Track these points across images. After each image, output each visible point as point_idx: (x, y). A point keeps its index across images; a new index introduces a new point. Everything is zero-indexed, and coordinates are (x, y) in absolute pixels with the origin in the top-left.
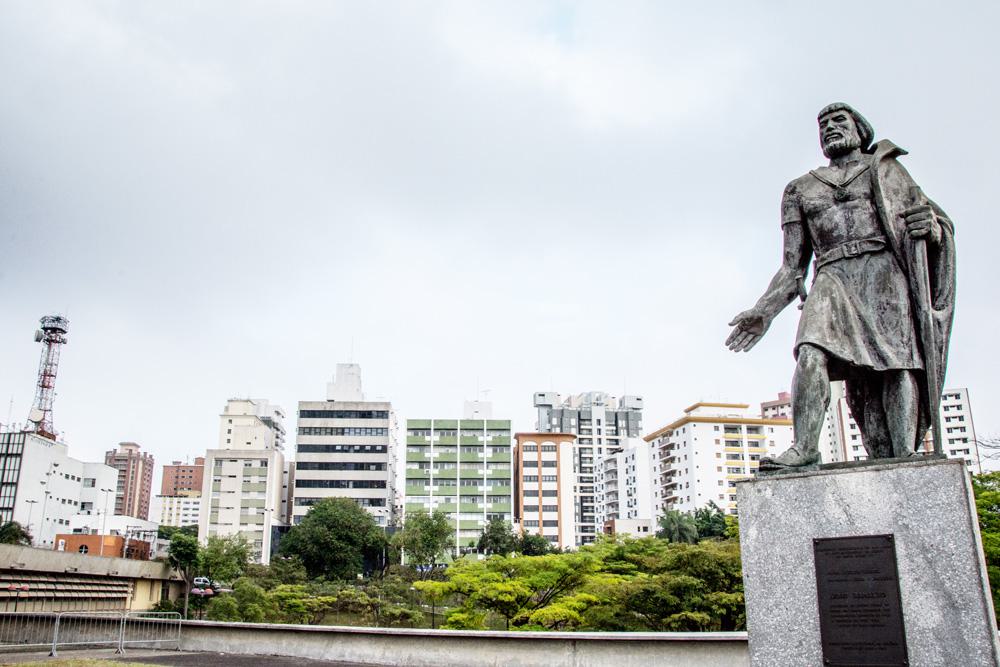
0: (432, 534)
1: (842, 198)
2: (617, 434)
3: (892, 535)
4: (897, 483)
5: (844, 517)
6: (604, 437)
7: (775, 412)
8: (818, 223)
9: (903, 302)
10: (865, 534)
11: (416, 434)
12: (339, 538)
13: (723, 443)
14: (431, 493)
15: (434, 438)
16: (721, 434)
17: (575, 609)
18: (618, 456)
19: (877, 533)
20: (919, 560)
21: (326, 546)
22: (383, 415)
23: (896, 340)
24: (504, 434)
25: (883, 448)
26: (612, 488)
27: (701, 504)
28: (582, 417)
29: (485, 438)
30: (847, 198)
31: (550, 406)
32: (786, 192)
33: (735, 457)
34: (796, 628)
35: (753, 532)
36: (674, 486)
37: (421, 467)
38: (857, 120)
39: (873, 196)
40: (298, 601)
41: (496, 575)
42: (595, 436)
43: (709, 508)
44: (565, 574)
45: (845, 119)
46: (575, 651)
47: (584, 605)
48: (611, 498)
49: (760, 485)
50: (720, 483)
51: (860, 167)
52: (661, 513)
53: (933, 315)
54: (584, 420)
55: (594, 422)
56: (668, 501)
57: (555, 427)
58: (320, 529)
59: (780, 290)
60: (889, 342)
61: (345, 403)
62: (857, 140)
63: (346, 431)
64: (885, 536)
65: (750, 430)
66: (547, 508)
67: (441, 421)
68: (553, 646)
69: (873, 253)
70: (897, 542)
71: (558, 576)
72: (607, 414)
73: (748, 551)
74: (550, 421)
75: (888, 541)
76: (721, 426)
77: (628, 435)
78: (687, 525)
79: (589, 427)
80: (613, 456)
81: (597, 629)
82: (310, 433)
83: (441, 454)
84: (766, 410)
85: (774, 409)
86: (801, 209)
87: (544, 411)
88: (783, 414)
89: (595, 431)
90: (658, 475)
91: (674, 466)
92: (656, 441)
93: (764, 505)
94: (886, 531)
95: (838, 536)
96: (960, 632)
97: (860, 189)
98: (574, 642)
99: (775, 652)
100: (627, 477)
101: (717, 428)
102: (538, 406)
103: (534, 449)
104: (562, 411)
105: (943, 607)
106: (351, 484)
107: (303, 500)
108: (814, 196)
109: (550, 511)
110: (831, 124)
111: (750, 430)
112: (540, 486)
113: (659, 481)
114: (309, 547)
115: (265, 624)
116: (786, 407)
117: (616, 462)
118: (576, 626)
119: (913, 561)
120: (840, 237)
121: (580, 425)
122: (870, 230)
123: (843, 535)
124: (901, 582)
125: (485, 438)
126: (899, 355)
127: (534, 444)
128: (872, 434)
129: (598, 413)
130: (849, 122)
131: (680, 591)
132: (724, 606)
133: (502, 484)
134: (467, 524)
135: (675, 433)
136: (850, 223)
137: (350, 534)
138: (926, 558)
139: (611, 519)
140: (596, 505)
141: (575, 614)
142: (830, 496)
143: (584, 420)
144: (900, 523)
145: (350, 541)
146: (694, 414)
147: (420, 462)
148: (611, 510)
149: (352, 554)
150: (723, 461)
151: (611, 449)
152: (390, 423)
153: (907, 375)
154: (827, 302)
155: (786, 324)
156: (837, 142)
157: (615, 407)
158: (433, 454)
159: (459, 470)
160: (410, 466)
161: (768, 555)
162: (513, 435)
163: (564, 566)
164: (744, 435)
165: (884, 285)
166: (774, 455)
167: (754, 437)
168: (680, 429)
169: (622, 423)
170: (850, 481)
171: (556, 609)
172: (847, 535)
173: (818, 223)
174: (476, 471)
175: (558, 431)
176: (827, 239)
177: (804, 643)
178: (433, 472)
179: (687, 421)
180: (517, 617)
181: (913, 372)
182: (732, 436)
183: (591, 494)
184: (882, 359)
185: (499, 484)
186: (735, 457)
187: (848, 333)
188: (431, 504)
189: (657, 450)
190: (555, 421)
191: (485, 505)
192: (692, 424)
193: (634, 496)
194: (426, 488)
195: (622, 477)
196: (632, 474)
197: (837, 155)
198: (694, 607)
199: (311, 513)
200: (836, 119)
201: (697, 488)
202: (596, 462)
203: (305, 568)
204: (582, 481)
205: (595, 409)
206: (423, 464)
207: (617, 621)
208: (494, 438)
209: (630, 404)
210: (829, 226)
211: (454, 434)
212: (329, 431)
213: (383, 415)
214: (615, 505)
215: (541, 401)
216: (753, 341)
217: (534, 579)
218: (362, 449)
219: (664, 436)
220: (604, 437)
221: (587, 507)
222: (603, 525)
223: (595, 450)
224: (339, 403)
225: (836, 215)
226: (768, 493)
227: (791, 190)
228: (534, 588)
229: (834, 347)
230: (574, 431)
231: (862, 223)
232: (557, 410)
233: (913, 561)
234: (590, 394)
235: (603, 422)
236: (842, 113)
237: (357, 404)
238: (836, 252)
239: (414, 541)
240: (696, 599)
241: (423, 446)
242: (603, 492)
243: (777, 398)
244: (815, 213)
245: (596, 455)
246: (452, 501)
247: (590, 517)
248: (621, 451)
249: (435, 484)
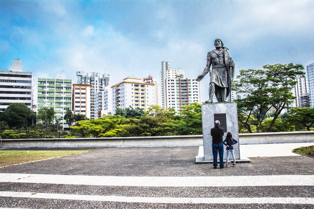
0: (50, 113)
1: (218, 56)
2: (102, 85)
4: (227, 106)
5: (219, 111)
6: (98, 86)
7: (147, 81)
8: (214, 60)
9: (226, 76)
11: (41, 83)
12: (20, 115)
13: (134, 89)
14: (46, 102)
15: (47, 84)
16: (134, 87)
17: (115, 133)
18: (102, 92)
20: (229, 117)
21: (15, 118)
22: (30, 76)
23: (225, 82)
24: (70, 84)
25: (221, 100)
26: (100, 101)
27: (127, 106)
28: (91, 80)
29: (64, 85)
30: (220, 57)
31: (82, 76)
32: (208, 53)
33: (137, 93)
35: (204, 113)
36: (119, 101)
37: (43, 93)
38: (222, 42)
39: (224, 57)
40: (13, 135)
41: (94, 124)
42: (95, 86)
43: (129, 108)
44: (111, 124)
46: (124, 142)
47: (117, 132)
48: (100, 104)
49: (206, 105)
50: (132, 101)
51: (222, 51)
52: (116, 109)
54: (92, 81)
55: (95, 81)
56: (117, 105)
57: (83, 82)
58: (13, 113)
59: (206, 71)
60: (224, 82)
61: (16, 72)
62: (221, 46)
63: (17, 81)
65: (142, 86)
66: (82, 107)
67: (49, 79)
68: (118, 141)
69: (223, 67)
71: (110, 124)
72: (99, 79)
74: (81, 80)
75: (225, 114)
76: (134, 84)
77: (105, 85)
78: (123, 112)
79: (93, 83)
80: (101, 92)
81: (122, 137)
82: (3, 82)
83: (49, 89)
85: (147, 80)
86: (211, 57)
87: (80, 77)
88: (149, 82)
89: (95, 84)
90: (115, 97)
91: (119, 95)
92: (114, 88)
93: (206, 108)
94: (225, 113)
97: (222, 56)
98: (123, 140)
100: (105, 98)
101: (132, 85)
102: (78, 75)
103: (79, 89)
104: (85, 77)
106: (19, 98)
107: (2, 103)
108: (214, 55)
109: (83, 107)
110: (218, 42)
112: (80, 100)
113: (115, 100)
114: (9, 118)
115: (22, 139)
116: (150, 80)
117: (101, 93)
118: (114, 136)
120: (218, 64)
121: (91, 82)
122: (223, 63)
125: (64, 85)
126: (225, 85)
127: (79, 87)
128: (218, 97)
129: (96, 79)
130: (220, 43)
131: (144, 127)
132: (154, 131)
133: (69, 99)
134: (60, 112)
135: (120, 86)
136: (219, 61)
137: (23, 114)
139: (100, 110)
140: (95, 106)
141: (115, 134)
143: (92, 81)
145: (23, 116)
146: (126, 81)
147: (42, 92)
148: (100, 108)
149: (24, 120)
150: (134, 95)
151: (100, 90)
152: (32, 79)
154: (215, 75)
155: (207, 77)
156: (218, 46)
157: (101, 77)
158: (47, 90)
159: (55, 95)
160: (39, 93)
162: (72, 84)
163: (112, 122)
164: (140, 88)
165: (224, 73)
167: (143, 88)
168: (122, 85)
169: (103, 82)
171: (109, 133)
173: (214, 60)
174: (61, 95)
175: (84, 83)
176: (215, 64)
178: (47, 95)
179: (124, 82)
180: (99, 135)
181: (227, 88)
182: (137, 88)
183: (93, 103)
184: (222, 85)
185: (68, 99)
186: (137, 93)
187: (218, 81)
188: (47, 104)
189: (115, 90)
190: (83, 80)
191: (64, 106)
192: (125, 83)
193: (107, 104)
194: (44, 100)
195: (103, 98)
196: (106, 97)
197: (218, 48)
198: (147, 132)
199: (8, 108)
200: (218, 42)
201: (126, 102)
202: (95, 93)
203: (8, 125)
204: (91, 99)
205: (95, 77)
206: (43, 93)
207: (125, 135)
208: (66, 85)
209: (106, 76)
210: (216, 61)
211: (54, 84)
212: (11, 81)
213: (30, 76)
214: (101, 106)
215: (79, 74)
216: (201, 80)
217: (103, 125)
218: (23, 87)
219: (117, 87)
220: (98, 86)
221: (92, 107)
222: (97, 112)
223: (95, 90)
224: (14, 72)
225: (217, 60)
226: (207, 106)
227: (209, 53)
228: (103, 127)
229: (217, 83)
230: (89, 84)
231: (222, 62)
232: (84, 77)
234: (94, 73)
235: (98, 81)
236: (220, 41)
237: (20, 72)
238: (217, 66)
239: (44, 116)
240: (148, 130)
241: (43, 87)
242: (97, 102)
243: (148, 77)
244: (214, 59)
245: (95, 91)
246: (53, 104)
247: (93, 109)
248: (103, 90)
249: (64, 99)
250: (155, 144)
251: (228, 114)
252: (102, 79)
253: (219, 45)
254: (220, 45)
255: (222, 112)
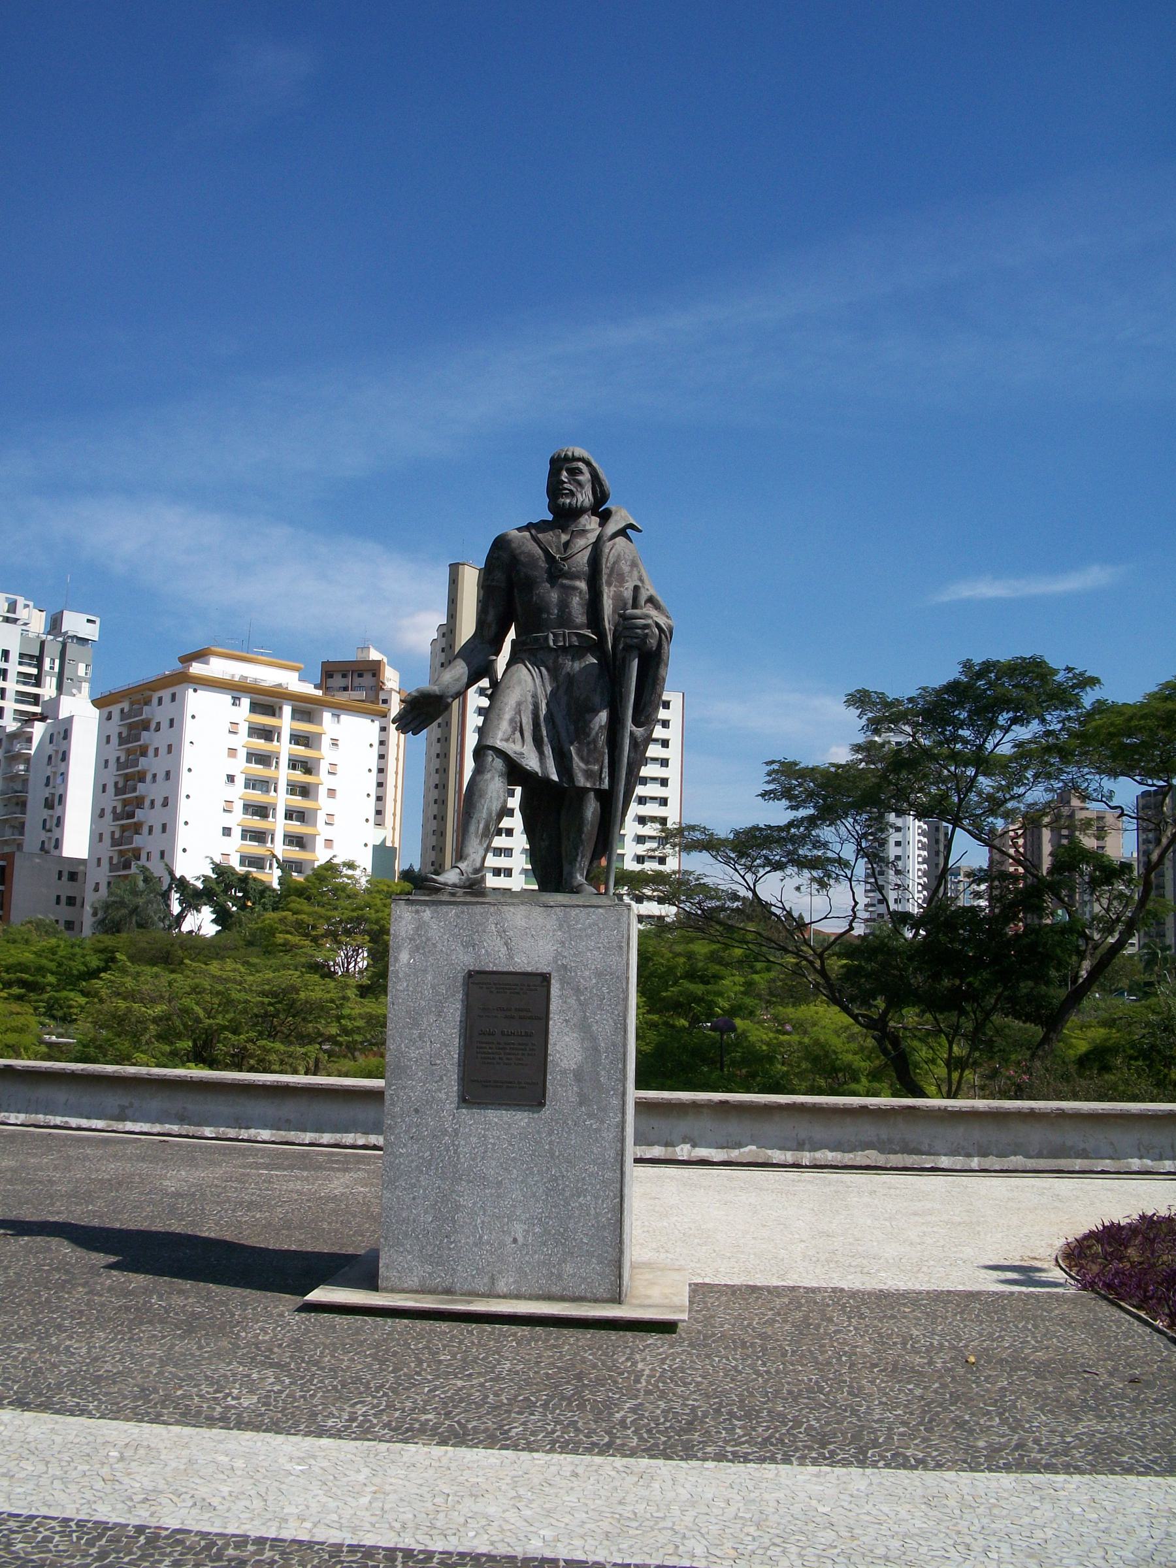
3: (550, 974)
5: (504, 950)
10: (523, 970)
19: (534, 971)
20: (572, 1001)
34: (438, 1062)
45: (581, 473)
53: (632, 733)
64: (542, 975)
70: (553, 981)
73: (397, 977)
75: (545, 978)
84: (331, 676)
85: (344, 676)
95: (495, 969)
96: (598, 1074)
99: (414, 1086)
105: (587, 1049)
111: (298, 714)
119: (565, 1002)
123: (500, 969)
124: (551, 1022)
130: (585, 477)
138: (578, 1000)
142: (493, 926)
144: (559, 962)
153: (592, 794)
161: (418, 983)
166: (233, 676)
170: (517, 917)
172: (505, 970)
177: (445, 1078)
233: (565, 1002)
236: (581, 465)
250: (783, 1157)
251: (563, 982)
252: (43, 643)
253: (572, 494)
254: (585, 497)
255: (523, 962)
